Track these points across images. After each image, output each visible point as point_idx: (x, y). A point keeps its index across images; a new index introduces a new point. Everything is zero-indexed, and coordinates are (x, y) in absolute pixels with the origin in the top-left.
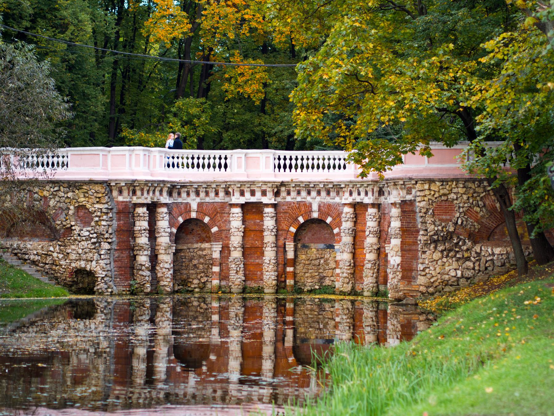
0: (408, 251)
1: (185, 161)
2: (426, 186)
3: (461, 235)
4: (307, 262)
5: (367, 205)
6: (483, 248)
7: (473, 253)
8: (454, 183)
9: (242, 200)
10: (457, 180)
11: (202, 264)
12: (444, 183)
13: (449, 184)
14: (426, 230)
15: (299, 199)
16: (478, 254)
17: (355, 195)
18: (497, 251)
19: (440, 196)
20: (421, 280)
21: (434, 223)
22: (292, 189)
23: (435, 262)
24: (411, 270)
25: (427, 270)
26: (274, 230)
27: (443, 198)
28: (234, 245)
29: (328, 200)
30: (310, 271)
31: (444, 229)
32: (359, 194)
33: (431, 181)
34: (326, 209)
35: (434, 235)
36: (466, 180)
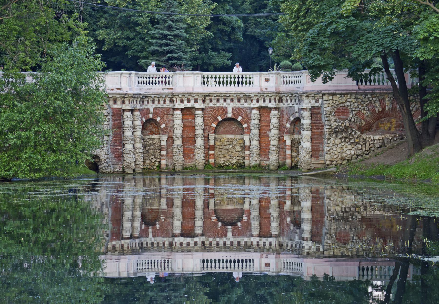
1: (160, 79)
2: (331, 98)
3: (353, 128)
4: (221, 147)
5: (271, 109)
6: (367, 136)
7: (361, 140)
8: (349, 96)
9: (182, 106)
10: (351, 94)
11: (153, 149)
12: (343, 96)
13: (345, 96)
14: (331, 125)
15: (218, 105)
16: (365, 140)
17: (261, 102)
18: (376, 138)
19: (340, 104)
20: (328, 157)
21: (335, 121)
22: (213, 98)
23: (336, 146)
24: (318, 151)
25: (331, 151)
26: (203, 126)
27: (341, 105)
28: (177, 136)
29: (239, 105)
30: (223, 153)
31: (343, 125)
32: (264, 101)
33: (333, 94)
34: (237, 111)
35: (336, 128)
36: (357, 94)
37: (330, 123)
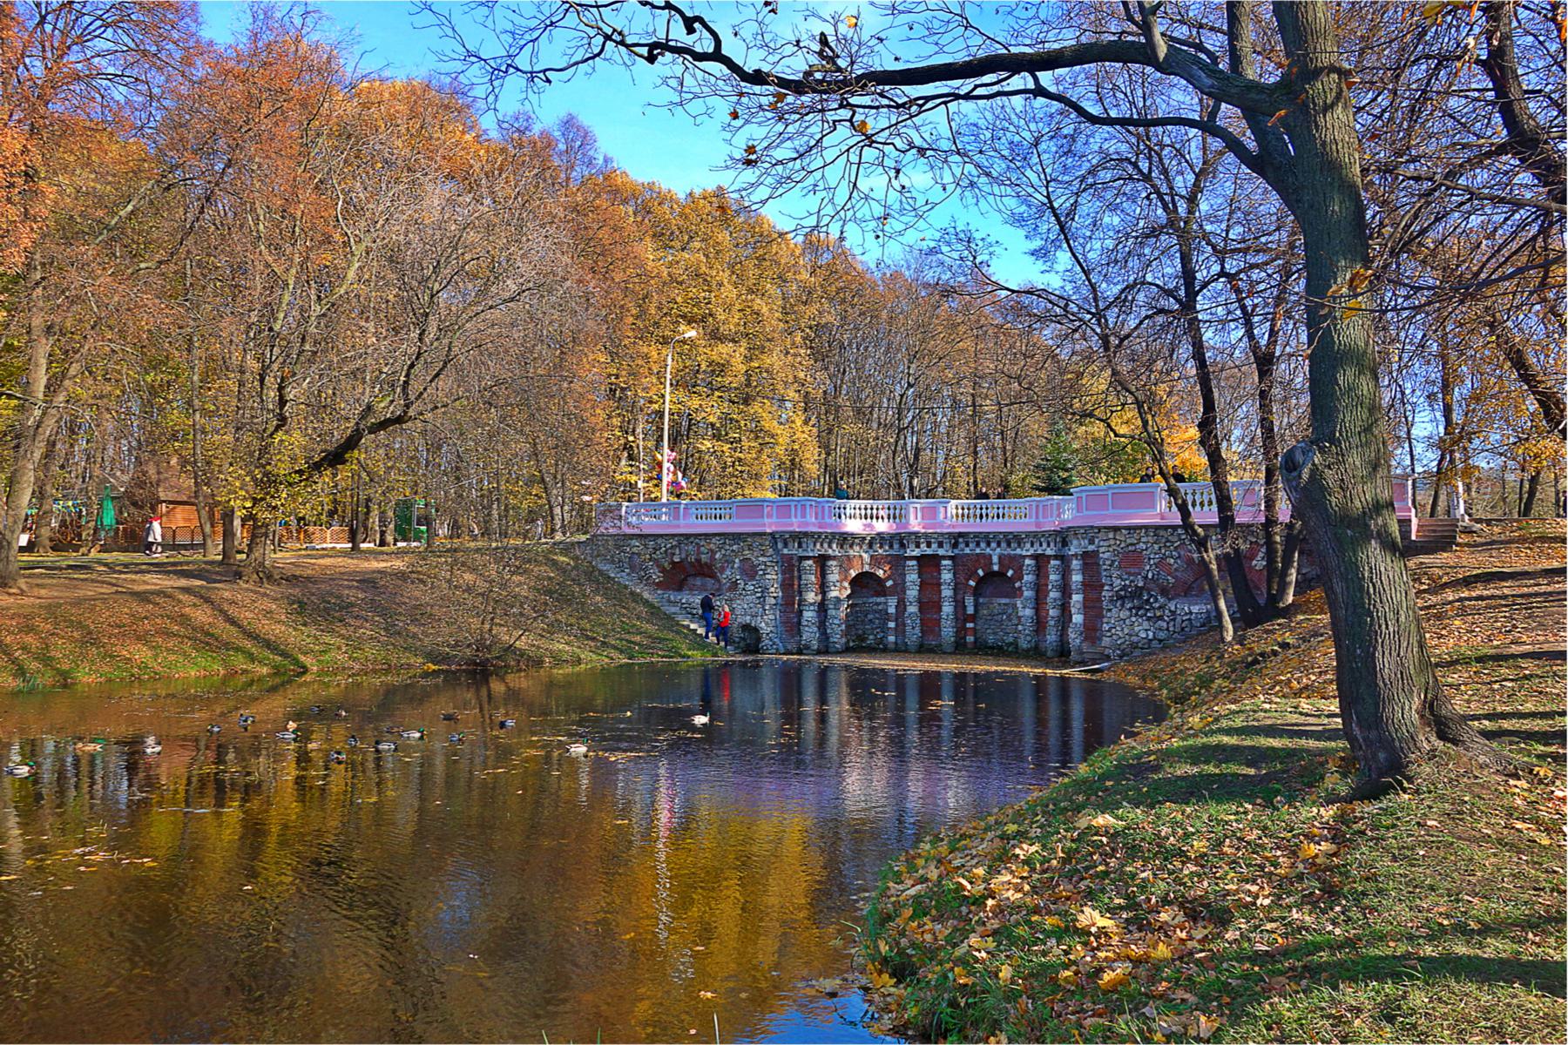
0: (1093, 609)
2: (1111, 535)
9: (916, 553)
16: (1173, 613)
17: (1037, 545)
18: (1195, 609)
20: (1106, 641)
24: (1095, 630)
29: (1009, 551)
37: (1115, 581)
